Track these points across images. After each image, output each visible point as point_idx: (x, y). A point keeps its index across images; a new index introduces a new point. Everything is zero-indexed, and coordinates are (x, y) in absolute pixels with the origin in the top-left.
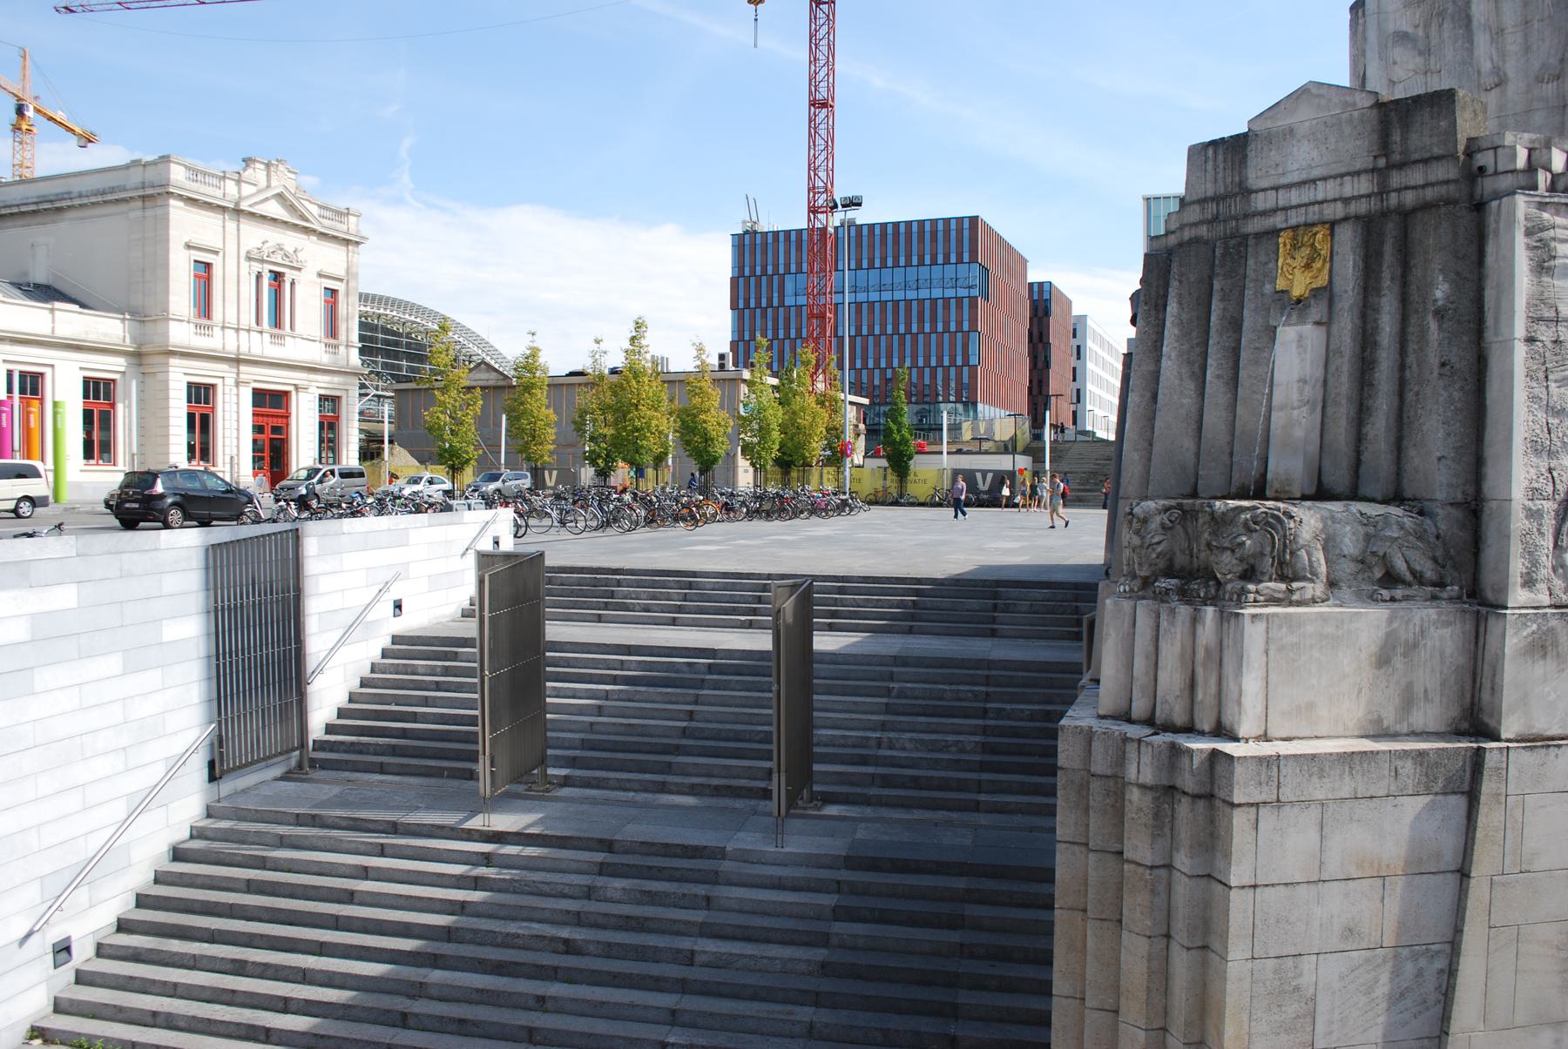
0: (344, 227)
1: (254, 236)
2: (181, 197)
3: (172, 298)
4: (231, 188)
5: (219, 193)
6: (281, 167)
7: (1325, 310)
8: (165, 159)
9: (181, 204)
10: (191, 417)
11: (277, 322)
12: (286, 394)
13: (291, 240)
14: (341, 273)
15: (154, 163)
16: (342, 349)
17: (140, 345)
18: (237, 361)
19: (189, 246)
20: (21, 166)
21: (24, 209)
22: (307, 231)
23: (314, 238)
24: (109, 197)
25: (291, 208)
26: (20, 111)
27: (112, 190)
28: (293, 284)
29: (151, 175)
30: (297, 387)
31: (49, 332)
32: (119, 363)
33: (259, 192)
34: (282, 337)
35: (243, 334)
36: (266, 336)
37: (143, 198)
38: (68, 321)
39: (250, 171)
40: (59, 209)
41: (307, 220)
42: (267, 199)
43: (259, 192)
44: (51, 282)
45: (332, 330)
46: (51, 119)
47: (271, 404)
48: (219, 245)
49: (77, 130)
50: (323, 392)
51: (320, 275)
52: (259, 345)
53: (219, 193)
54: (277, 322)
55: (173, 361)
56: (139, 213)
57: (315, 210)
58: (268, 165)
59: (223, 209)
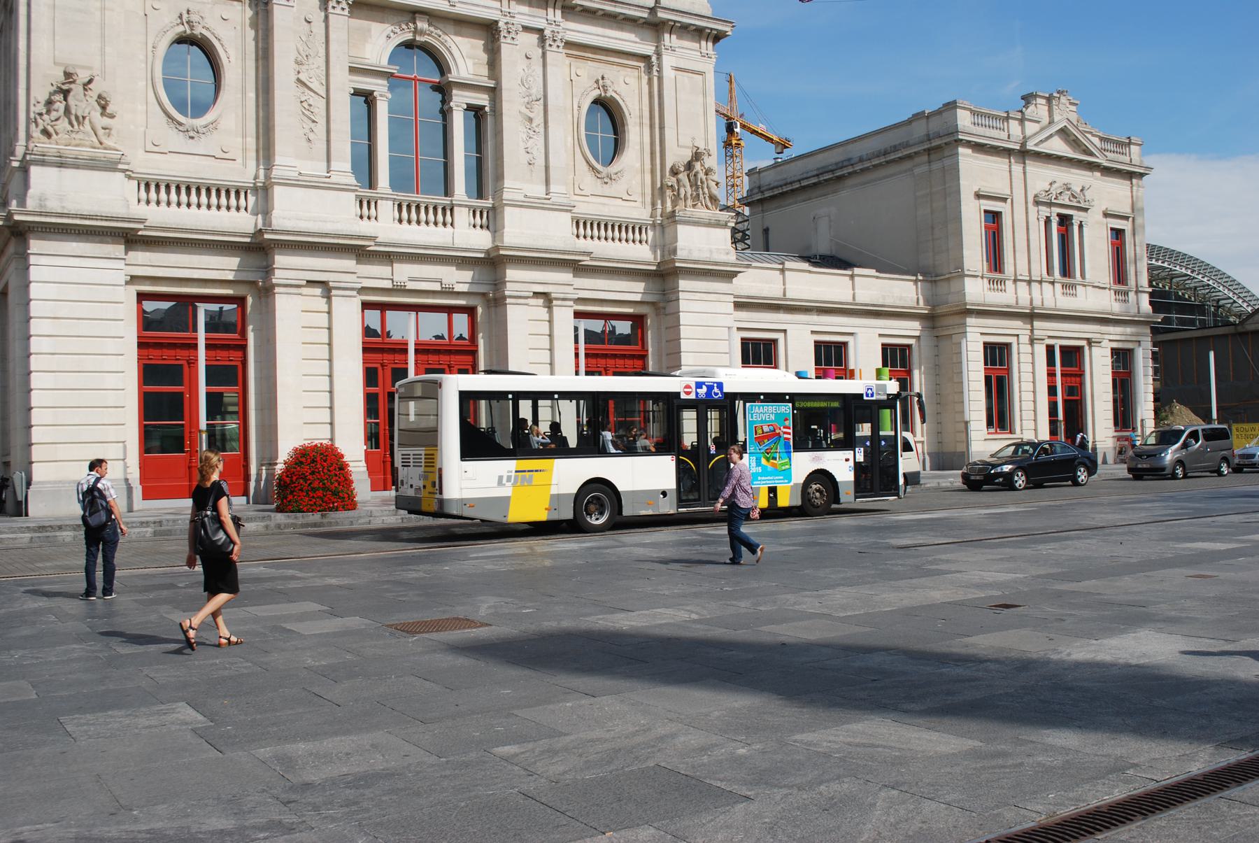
0: (1126, 159)
1: (1042, 177)
2: (969, 144)
3: (966, 253)
4: (1014, 127)
5: (1004, 135)
6: (1063, 100)
7: (377, 523)
8: (951, 106)
9: (969, 151)
10: (988, 380)
11: (1066, 271)
12: (1079, 349)
13: (1077, 178)
14: (1125, 209)
15: (938, 112)
16: (1132, 295)
17: (934, 307)
18: (1031, 316)
19: (978, 196)
20: (733, 177)
21: (804, 183)
22: (1092, 167)
23: (1098, 174)
24: (892, 157)
25: (1075, 143)
26: (730, 128)
27: (895, 149)
28: (1081, 226)
29: (935, 125)
30: (1089, 341)
31: (850, 300)
32: (912, 328)
33: (1042, 129)
34: (1073, 286)
35: (1035, 286)
36: (1058, 286)
37: (929, 151)
38: (870, 287)
39: (1032, 108)
40: (840, 178)
41: (1091, 154)
42: (1051, 136)
43: (1042, 129)
44: (834, 253)
45: (1120, 275)
46: (754, 132)
47: (1070, 359)
48: (1006, 192)
49: (775, 138)
50: (1115, 345)
51: (1106, 215)
52: (1051, 297)
53: (1004, 135)
54: (1066, 271)
55: (970, 321)
56: (925, 168)
57: (1096, 141)
58: (1049, 100)
59: (1007, 152)
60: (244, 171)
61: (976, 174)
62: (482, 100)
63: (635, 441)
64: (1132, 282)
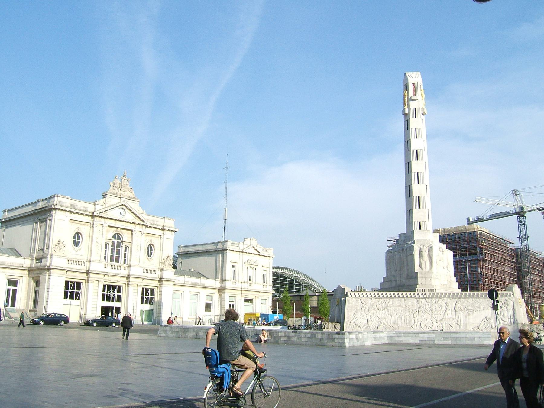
1: (247, 257)
52: (246, 286)
60: (84, 258)
61: (230, 256)
62: (129, 244)
63: (213, 384)
64: (268, 283)
